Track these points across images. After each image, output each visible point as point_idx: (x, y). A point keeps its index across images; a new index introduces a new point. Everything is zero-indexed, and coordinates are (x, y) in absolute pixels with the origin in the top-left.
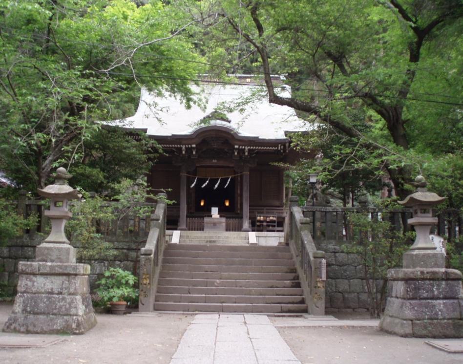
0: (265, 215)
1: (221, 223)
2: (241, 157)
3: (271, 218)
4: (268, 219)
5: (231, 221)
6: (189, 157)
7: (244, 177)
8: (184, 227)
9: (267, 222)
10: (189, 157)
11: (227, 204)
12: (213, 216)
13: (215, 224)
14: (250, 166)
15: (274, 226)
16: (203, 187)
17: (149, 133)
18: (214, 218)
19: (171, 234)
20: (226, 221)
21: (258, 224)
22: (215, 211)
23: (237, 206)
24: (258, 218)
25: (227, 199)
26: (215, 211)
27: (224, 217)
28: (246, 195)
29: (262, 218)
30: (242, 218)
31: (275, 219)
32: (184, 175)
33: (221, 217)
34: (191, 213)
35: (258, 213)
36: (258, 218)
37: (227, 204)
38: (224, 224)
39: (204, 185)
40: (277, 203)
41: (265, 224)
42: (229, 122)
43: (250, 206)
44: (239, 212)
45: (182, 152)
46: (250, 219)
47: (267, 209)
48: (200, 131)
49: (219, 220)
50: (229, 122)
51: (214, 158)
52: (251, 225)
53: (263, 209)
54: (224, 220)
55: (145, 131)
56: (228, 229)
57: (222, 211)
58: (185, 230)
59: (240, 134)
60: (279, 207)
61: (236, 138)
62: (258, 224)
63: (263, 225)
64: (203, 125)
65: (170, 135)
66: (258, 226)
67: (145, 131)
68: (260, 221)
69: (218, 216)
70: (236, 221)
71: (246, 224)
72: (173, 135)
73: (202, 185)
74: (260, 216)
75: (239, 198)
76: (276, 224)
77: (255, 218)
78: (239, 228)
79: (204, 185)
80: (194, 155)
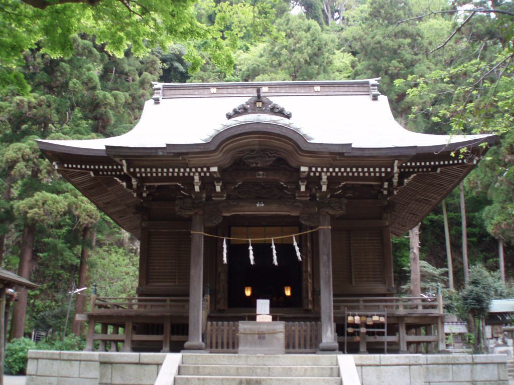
0: (361, 313)
1: (274, 333)
2: (313, 197)
3: (376, 318)
4: (369, 322)
5: (296, 326)
6: (209, 198)
7: (321, 238)
8: (199, 341)
9: (367, 326)
10: (209, 198)
11: (288, 293)
12: (259, 319)
13: (261, 336)
14: (331, 212)
15: (382, 334)
16: (252, 262)
17: (353, 146)
18: (260, 323)
19: (157, 360)
20: (286, 327)
21: (350, 330)
22: (263, 306)
23: (308, 297)
24: (350, 319)
25: (248, 285)
26: (263, 306)
27: (282, 319)
28: (326, 272)
29: (357, 319)
30: (318, 319)
31: (382, 319)
32: (199, 235)
33: (274, 319)
34: (220, 311)
35: (350, 308)
36: (350, 319)
37: (288, 293)
38: (282, 336)
39: (252, 257)
40: (381, 288)
41: (363, 330)
42: (288, 116)
43: (334, 296)
44: (310, 307)
45: (320, 188)
46: (335, 321)
47: (365, 301)
48: (289, 135)
49: (271, 327)
50: (288, 116)
51: (260, 199)
52: (336, 334)
53: (358, 301)
54: (280, 326)
55: (350, 144)
56: (291, 346)
57: (279, 308)
58: (199, 348)
59: (311, 139)
60: (384, 295)
61: (304, 147)
62: (350, 330)
63: (359, 333)
64: (233, 122)
65: (163, 145)
66: (349, 334)
67: (350, 144)
68: (354, 325)
69: (269, 318)
70: (306, 326)
71: (329, 336)
72: (417, 154)
73: (223, 261)
74: (354, 316)
75: (310, 281)
76: (385, 330)
77: (344, 318)
78: (312, 344)
79: (252, 257)
80: (302, 195)
